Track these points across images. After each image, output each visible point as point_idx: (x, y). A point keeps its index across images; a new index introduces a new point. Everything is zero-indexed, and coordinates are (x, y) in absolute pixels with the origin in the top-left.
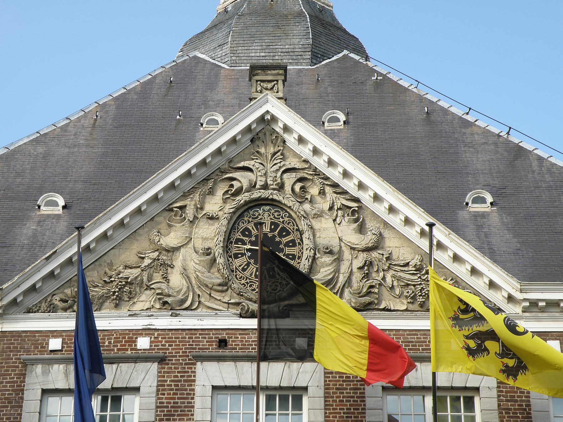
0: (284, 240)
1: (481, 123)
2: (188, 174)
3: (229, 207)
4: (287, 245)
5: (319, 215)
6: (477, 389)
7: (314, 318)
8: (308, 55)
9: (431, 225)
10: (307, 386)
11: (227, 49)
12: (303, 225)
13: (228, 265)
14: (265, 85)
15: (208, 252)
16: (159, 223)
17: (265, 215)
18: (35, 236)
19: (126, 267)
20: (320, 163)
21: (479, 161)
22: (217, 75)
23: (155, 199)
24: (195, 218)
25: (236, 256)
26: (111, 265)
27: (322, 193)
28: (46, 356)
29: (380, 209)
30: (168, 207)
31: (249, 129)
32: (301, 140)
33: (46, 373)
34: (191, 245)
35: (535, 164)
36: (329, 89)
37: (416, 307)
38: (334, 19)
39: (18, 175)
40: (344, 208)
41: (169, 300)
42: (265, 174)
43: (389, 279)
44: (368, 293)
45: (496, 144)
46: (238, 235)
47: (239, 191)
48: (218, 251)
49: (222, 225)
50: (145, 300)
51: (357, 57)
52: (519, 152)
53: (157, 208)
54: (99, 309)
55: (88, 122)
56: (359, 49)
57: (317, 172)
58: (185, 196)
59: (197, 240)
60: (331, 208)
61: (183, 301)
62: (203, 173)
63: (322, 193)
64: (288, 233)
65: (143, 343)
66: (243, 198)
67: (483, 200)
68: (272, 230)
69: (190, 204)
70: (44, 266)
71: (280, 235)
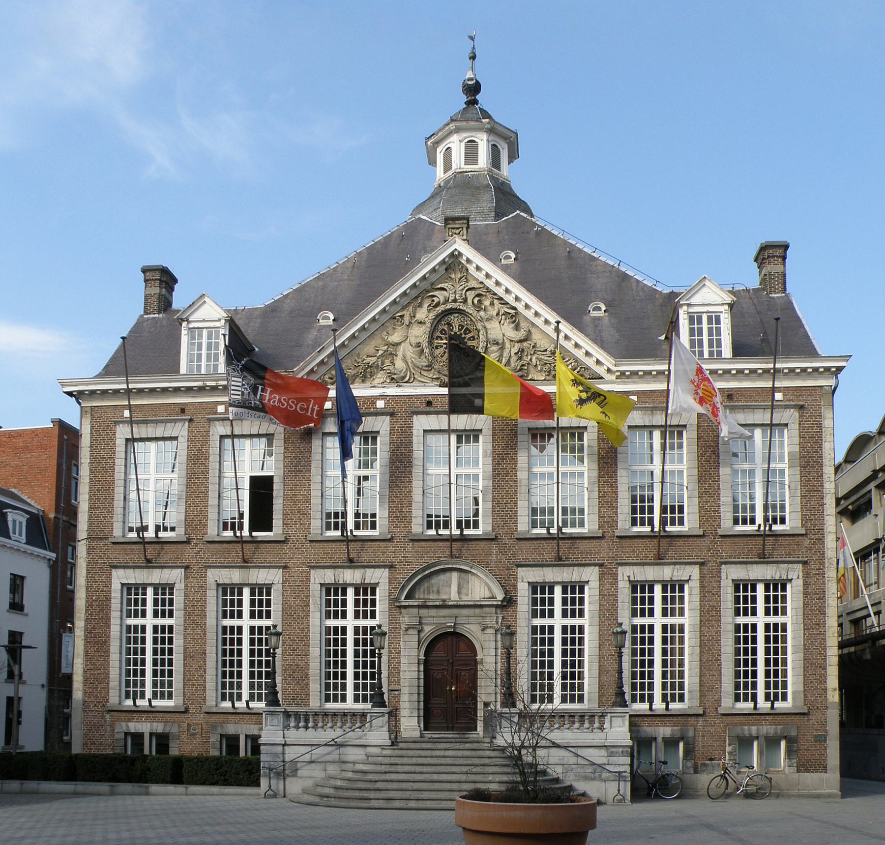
0: (468, 336)
1: (602, 259)
2: (404, 294)
3: (432, 315)
4: (469, 339)
5: (489, 319)
6: (586, 428)
7: (483, 386)
8: (493, 214)
9: (558, 322)
11: (439, 211)
12: (479, 326)
13: (432, 354)
15: (418, 345)
16: (388, 327)
17: (455, 320)
18: (316, 339)
19: (368, 356)
20: (490, 284)
21: (599, 283)
22: (433, 230)
23: (384, 311)
24: (410, 323)
25: (437, 348)
26: (358, 355)
27: (492, 304)
29: (529, 314)
30: (392, 318)
31: (443, 262)
32: (478, 268)
34: (408, 341)
36: (506, 237)
37: (550, 377)
38: (511, 189)
39: (307, 300)
40: (506, 313)
41: (395, 377)
42: (455, 292)
43: (534, 360)
44: (521, 370)
45: (611, 272)
46: (438, 334)
47: (438, 304)
48: (425, 344)
49: (427, 328)
50: (380, 377)
51: (525, 215)
52: (625, 277)
53: (386, 317)
54: (353, 383)
55: (350, 265)
56: (528, 210)
57: (488, 290)
58: (403, 308)
59: (412, 336)
60: (498, 314)
61: (404, 377)
62: (415, 293)
63: (492, 304)
64: (470, 332)
65: (380, 404)
66: (440, 309)
67: (599, 309)
68: (460, 330)
69: (407, 314)
70: (317, 356)
71: (465, 333)
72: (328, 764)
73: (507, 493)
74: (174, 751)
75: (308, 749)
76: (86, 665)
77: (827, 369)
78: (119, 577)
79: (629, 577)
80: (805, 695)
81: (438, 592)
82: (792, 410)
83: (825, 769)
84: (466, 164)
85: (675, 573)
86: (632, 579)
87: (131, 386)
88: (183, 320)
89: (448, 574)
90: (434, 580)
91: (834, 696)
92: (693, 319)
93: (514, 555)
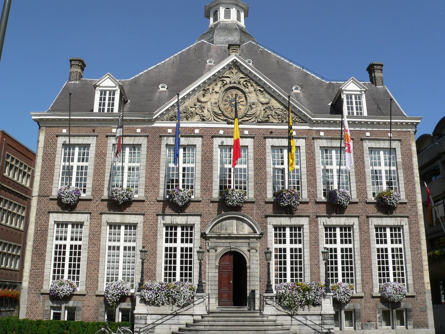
3: (223, 89)
10: (90, 144)
14: (234, 51)
18: (159, 97)
28: (167, 134)
30: (204, 89)
33: (167, 140)
35: (312, 78)
41: (204, 118)
47: (226, 84)
50: (197, 118)
61: (209, 119)
65: (197, 131)
72: (172, 326)
73: (261, 178)
74: (78, 318)
75: (160, 317)
76: (31, 267)
77: (412, 123)
78: (54, 217)
79: (323, 223)
80: (414, 286)
81: (226, 229)
82: (397, 142)
83: (427, 326)
84: (225, 18)
85: (346, 221)
86: (325, 224)
87: (71, 117)
88: (97, 86)
89: (231, 221)
90: (224, 222)
91: (428, 287)
92: (103, 93)
93: (265, 210)
